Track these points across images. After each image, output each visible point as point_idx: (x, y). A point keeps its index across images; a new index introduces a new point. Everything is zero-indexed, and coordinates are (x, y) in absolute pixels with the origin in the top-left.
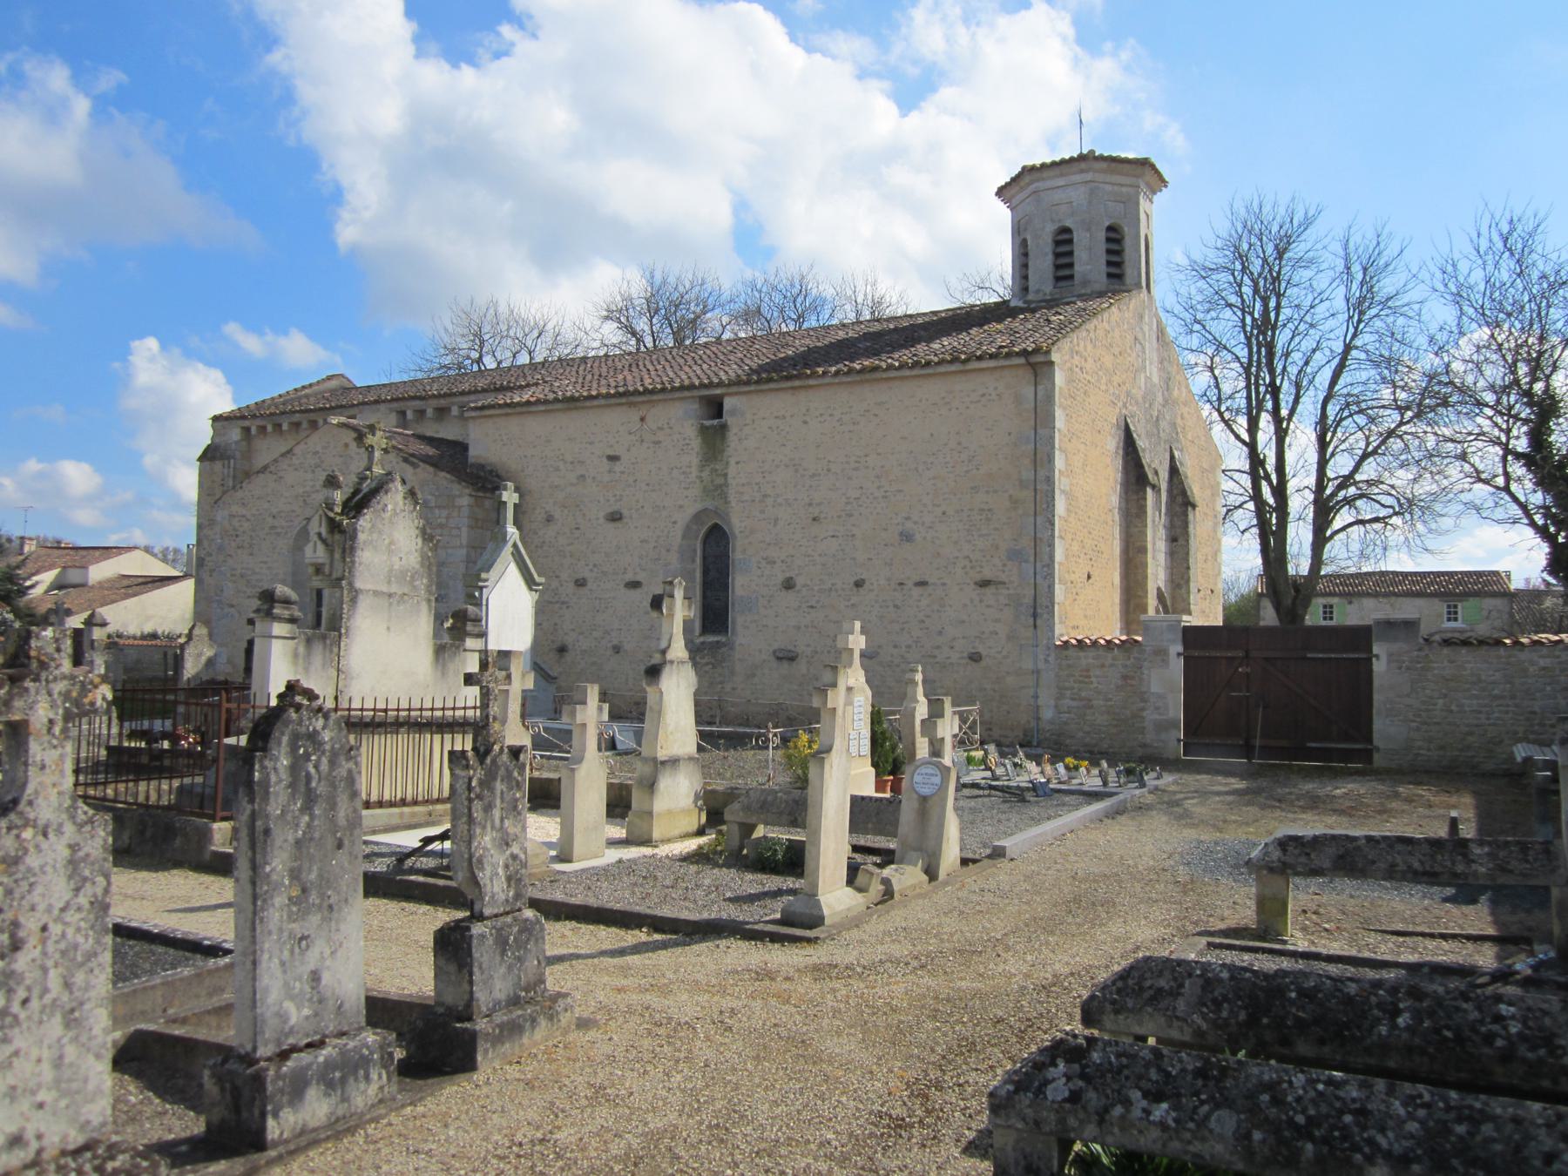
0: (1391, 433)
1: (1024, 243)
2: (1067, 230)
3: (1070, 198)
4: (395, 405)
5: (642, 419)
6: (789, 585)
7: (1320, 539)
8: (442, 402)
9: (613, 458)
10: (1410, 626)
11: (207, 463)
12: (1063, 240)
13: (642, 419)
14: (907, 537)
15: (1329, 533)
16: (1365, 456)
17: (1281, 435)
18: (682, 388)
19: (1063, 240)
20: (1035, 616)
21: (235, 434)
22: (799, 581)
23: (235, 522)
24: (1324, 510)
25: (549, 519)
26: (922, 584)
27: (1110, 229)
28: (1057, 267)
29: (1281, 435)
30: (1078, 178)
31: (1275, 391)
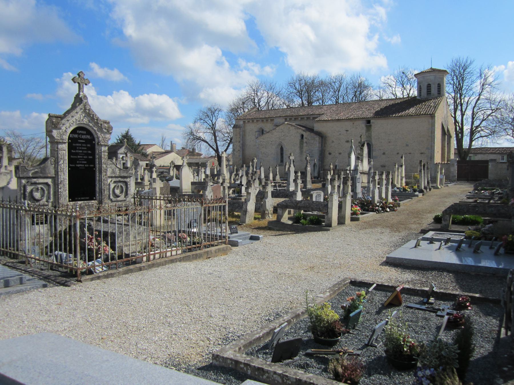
0: (489, 115)
1: (420, 86)
2: (429, 84)
3: (431, 77)
4: (285, 117)
5: (353, 124)
6: (384, 154)
7: (471, 141)
8: (291, 117)
9: (347, 131)
10: (495, 160)
11: (235, 129)
12: (429, 86)
13: (353, 124)
14: (407, 145)
15: (474, 139)
16: (483, 120)
17: (463, 115)
18: (362, 118)
19: (429, 86)
20: (431, 159)
21: (241, 123)
22: (386, 153)
23: (262, 143)
24: (472, 133)
25: (333, 142)
26: (410, 153)
27: (439, 84)
28: (428, 92)
29: (463, 115)
30: (432, 74)
31: (461, 105)
